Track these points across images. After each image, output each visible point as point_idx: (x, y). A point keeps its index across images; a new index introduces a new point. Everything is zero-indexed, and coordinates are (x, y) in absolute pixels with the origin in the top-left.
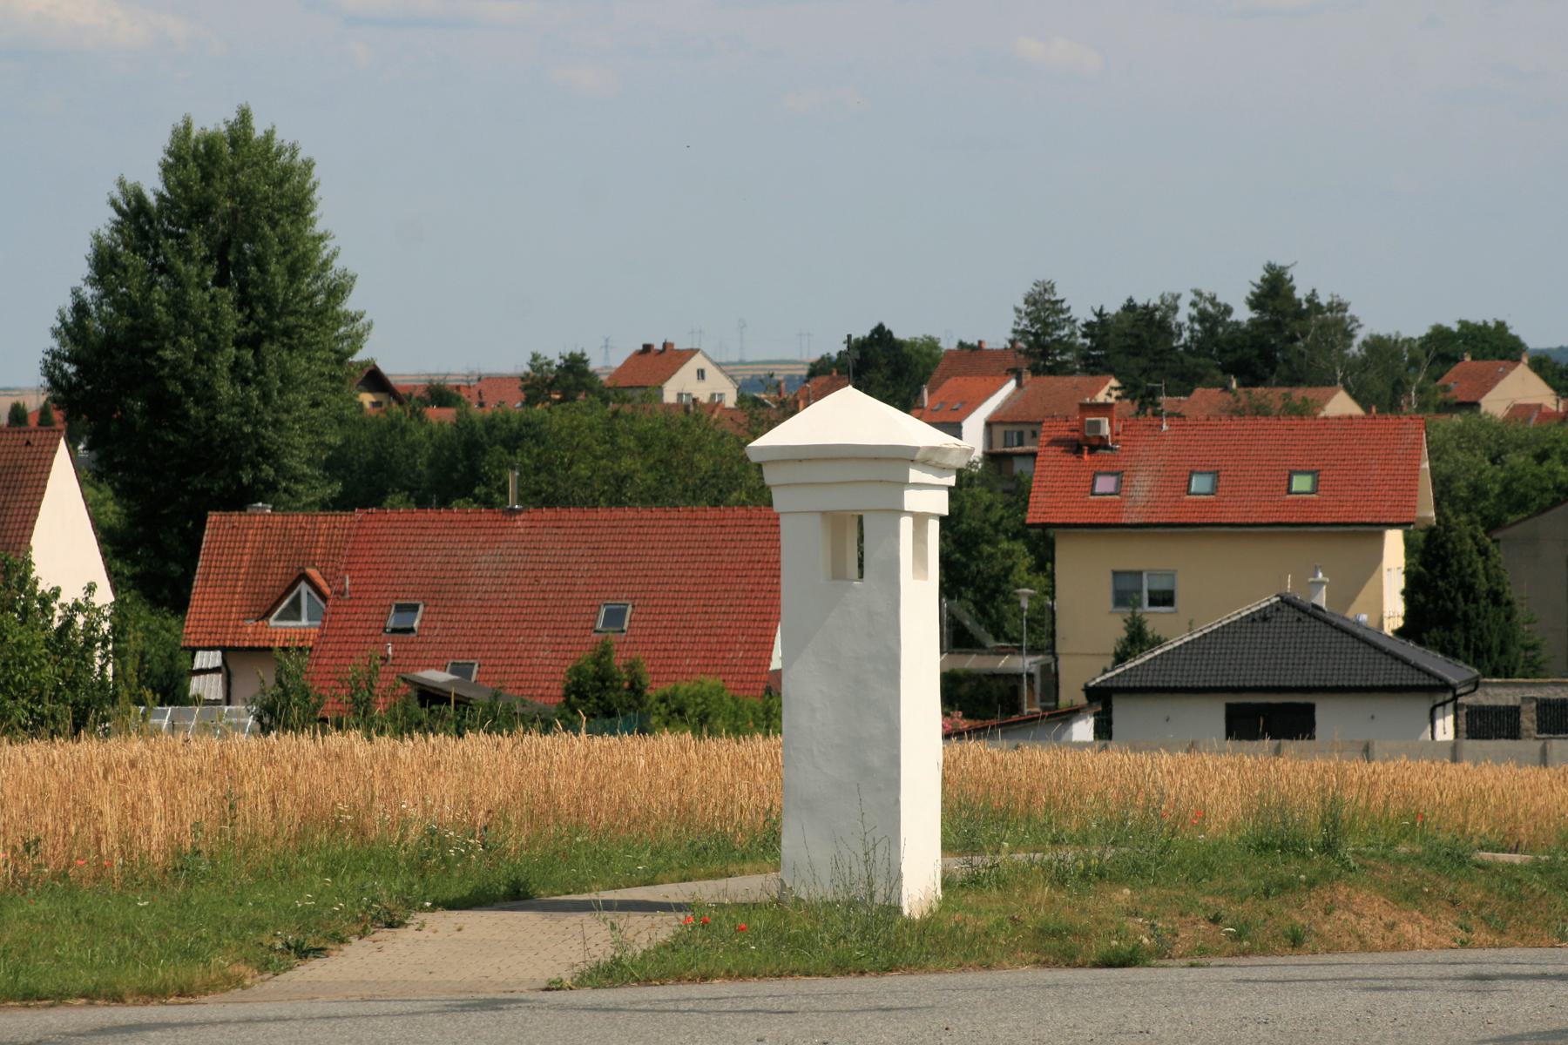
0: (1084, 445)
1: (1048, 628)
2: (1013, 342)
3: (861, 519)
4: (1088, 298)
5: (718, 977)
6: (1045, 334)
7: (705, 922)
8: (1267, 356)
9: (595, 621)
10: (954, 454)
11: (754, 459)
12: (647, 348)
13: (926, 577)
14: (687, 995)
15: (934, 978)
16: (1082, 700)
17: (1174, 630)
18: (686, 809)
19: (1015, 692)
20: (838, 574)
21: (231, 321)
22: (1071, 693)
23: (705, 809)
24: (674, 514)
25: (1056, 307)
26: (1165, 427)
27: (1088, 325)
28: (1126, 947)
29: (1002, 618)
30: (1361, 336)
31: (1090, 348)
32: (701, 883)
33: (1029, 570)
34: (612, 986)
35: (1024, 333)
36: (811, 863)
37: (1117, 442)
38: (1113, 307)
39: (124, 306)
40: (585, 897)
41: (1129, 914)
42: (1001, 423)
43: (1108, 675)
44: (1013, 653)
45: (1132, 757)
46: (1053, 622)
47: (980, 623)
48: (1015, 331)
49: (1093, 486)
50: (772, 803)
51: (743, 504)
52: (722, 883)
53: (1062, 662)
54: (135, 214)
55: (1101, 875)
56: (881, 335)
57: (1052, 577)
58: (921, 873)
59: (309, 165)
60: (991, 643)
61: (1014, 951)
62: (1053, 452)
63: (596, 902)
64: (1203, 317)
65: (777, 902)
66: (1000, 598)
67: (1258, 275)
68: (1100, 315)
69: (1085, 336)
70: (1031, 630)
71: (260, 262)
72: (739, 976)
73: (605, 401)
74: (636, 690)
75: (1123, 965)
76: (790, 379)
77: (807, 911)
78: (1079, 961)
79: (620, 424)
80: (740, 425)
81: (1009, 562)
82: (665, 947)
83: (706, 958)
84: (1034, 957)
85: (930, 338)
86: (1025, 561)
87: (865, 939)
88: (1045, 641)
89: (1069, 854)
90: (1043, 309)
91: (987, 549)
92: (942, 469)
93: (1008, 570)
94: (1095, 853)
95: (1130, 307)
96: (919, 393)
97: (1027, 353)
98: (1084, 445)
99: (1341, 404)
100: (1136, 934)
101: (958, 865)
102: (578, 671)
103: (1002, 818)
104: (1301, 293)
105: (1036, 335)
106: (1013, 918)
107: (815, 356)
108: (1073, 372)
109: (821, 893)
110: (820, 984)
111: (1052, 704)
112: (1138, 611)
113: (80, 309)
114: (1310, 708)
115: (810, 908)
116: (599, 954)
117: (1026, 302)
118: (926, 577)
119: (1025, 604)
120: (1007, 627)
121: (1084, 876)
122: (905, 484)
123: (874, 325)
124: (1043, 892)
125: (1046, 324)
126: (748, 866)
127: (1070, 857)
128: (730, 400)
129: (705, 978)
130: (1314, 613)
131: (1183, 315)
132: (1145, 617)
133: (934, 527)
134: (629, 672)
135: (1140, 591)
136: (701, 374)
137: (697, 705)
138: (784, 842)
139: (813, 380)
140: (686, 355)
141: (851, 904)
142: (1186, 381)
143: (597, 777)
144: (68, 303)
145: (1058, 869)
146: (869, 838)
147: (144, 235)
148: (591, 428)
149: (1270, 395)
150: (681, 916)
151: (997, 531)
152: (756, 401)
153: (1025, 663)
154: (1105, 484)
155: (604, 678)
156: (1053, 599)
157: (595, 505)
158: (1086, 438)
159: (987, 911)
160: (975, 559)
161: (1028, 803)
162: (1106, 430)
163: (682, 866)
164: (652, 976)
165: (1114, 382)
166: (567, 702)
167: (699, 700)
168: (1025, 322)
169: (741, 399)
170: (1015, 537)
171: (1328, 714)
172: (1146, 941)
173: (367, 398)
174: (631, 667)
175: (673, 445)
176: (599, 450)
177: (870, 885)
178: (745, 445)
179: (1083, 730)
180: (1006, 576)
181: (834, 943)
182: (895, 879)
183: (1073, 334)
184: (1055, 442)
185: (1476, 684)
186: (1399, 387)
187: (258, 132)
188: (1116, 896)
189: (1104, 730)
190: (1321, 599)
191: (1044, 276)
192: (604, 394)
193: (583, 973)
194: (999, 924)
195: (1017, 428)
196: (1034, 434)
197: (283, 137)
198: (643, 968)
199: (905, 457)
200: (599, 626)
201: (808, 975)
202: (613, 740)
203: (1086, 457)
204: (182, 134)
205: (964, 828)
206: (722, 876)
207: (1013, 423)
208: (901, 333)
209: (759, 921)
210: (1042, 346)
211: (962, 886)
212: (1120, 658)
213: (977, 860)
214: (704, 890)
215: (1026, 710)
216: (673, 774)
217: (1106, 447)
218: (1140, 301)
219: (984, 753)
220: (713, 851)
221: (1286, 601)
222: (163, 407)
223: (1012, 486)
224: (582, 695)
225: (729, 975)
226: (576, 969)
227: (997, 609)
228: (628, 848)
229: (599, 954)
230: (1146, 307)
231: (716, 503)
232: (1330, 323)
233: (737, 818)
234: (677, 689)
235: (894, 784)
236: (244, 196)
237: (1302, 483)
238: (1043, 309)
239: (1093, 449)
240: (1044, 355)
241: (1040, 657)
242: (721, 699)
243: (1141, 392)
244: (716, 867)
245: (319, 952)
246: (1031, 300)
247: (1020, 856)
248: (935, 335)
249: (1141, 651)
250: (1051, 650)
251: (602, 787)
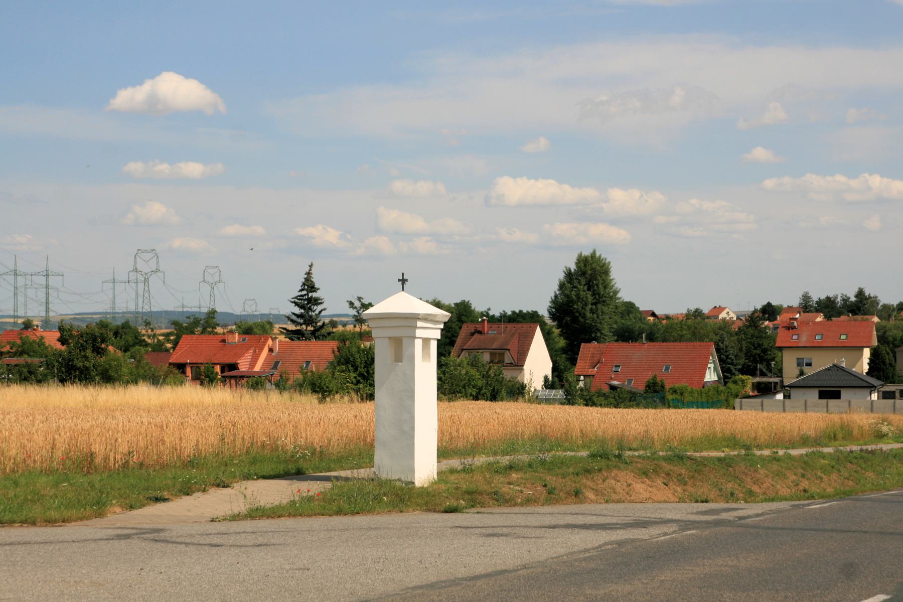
4: (817, 295)
8: (859, 309)
17: (809, 371)
21: (590, 299)
25: (809, 298)
30: (881, 304)
38: (823, 297)
39: (567, 296)
54: (569, 275)
56: (769, 304)
58: (425, 468)
59: (609, 263)
64: (844, 300)
67: (857, 290)
71: (597, 285)
74: (663, 386)
75: (451, 512)
87: (402, 496)
90: (806, 298)
99: (876, 319)
102: (648, 382)
104: (867, 294)
113: (556, 296)
114: (839, 392)
122: (416, 327)
128: (735, 319)
130: (842, 369)
131: (839, 299)
140: (724, 309)
142: (839, 314)
144: (553, 295)
147: (571, 279)
149: (859, 317)
153: (777, 380)
154: (795, 337)
162: (796, 324)
171: (844, 394)
173: (652, 318)
174: (661, 381)
175: (696, 328)
179: (780, 396)
185: (883, 385)
186: (890, 316)
187: (598, 255)
190: (844, 365)
197: (603, 256)
204: (580, 255)
208: (773, 304)
221: (835, 365)
222: (575, 320)
232: (874, 301)
236: (594, 270)
237: (843, 337)
238: (806, 298)
245: (165, 500)
250: (782, 376)
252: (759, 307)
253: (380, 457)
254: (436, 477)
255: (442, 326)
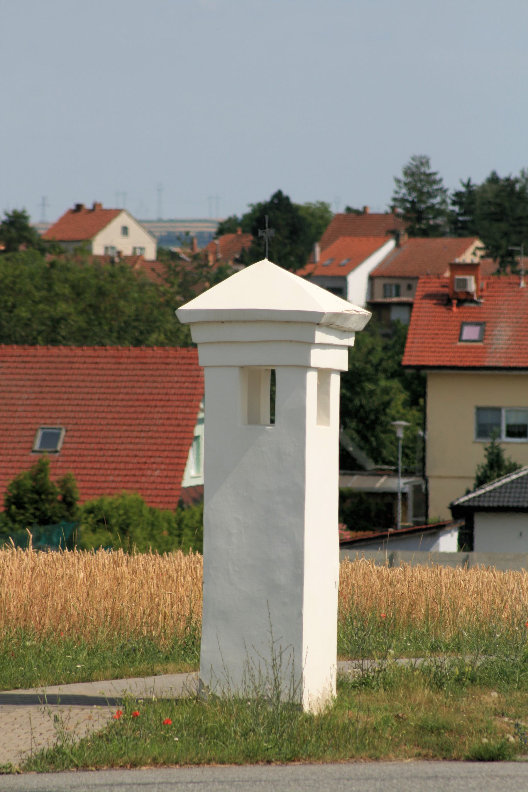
0: (453, 298)
1: (419, 455)
2: (393, 208)
3: (273, 373)
4: (457, 172)
5: (145, 764)
6: (420, 201)
7: (136, 715)
9: (32, 442)
10: (353, 319)
11: (183, 319)
12: (79, 207)
13: (328, 424)
14: (120, 780)
15: (331, 768)
16: (448, 516)
18: (117, 617)
19: (390, 508)
20: (253, 419)
22: (438, 511)
23: (134, 616)
24: (102, 353)
25: (430, 179)
26: (523, 284)
27: (458, 194)
28: (494, 744)
29: (381, 444)
31: (459, 214)
32: (131, 681)
33: (405, 404)
34: (54, 771)
35: (403, 200)
36: (225, 666)
37: (481, 297)
38: (479, 179)
40: (30, 692)
41: (496, 714)
42: (382, 277)
43: (471, 496)
44: (389, 475)
45: (497, 574)
46: (424, 449)
47: (361, 448)
48: (395, 199)
49: (461, 334)
50: (192, 612)
51: (161, 345)
52: (150, 681)
53: (432, 484)
55: (473, 680)
56: (280, 201)
57: (423, 410)
58: (319, 675)
60: (371, 465)
61: (398, 745)
62: (428, 304)
63: (42, 697)
65: (196, 698)
66: (379, 428)
68: (468, 185)
69: (454, 203)
70: (405, 455)
72: (164, 763)
73: (43, 251)
74: (68, 502)
75: (492, 759)
76: (200, 235)
77: (222, 706)
78: (454, 754)
79: (55, 273)
80: (159, 275)
81: (386, 398)
82: (100, 737)
83: (135, 748)
84: (416, 751)
85: (323, 204)
86: (403, 396)
87: (278, 731)
88: (417, 465)
89: (445, 660)
90: (419, 180)
91: (369, 386)
92: (343, 332)
93: (387, 404)
94: (467, 661)
95: (494, 179)
96: (311, 250)
97: (405, 217)
98: (453, 298)
100: (503, 732)
101: (351, 669)
102: (18, 485)
103: (388, 627)
105: (413, 203)
106: (397, 716)
107: (223, 216)
108: (443, 235)
109: (233, 690)
110: (233, 772)
111: (422, 519)
112: (497, 441)
115: (223, 704)
116: (43, 742)
117: (406, 174)
118: (328, 424)
119: (400, 434)
120: (385, 453)
121: (458, 680)
122: (311, 344)
123: (273, 191)
124: (423, 693)
125: (421, 193)
126: (171, 666)
127: (447, 664)
128: (150, 254)
129: (134, 765)
132: (503, 447)
133: (335, 381)
134: (62, 487)
135: (499, 425)
136: (125, 230)
137: (120, 515)
138: (203, 647)
139: (222, 238)
140: (115, 213)
141: (261, 702)
143: (43, 587)
145: (436, 674)
146: (277, 647)
148: (32, 277)
150: (114, 709)
151: (377, 370)
152: (174, 256)
153: (400, 484)
154: (471, 333)
155: (40, 491)
156: (424, 429)
157: (33, 344)
158: (455, 293)
159: (376, 709)
160: (358, 394)
161: (409, 614)
162: (472, 287)
163: (114, 666)
164: (89, 762)
165: (478, 243)
166: (8, 512)
167: (121, 512)
168: (404, 191)
169: (160, 252)
170: (393, 375)
172: (512, 739)
174: (64, 483)
175: (101, 293)
176: (37, 295)
177: (277, 687)
178: (175, 309)
179: (449, 542)
180: (384, 410)
181: (245, 735)
182: (297, 680)
183: (444, 202)
184: (429, 296)
188: (486, 698)
189: (466, 542)
191: (420, 152)
192: (43, 246)
193: (29, 759)
194: (386, 722)
195: (394, 282)
196: (409, 287)
198: (80, 756)
199: (312, 321)
200: (37, 447)
201: (222, 763)
202: (56, 555)
203: (455, 309)
205: (357, 635)
206: (148, 675)
207: (390, 277)
209: (182, 715)
210: (418, 213)
211: (354, 687)
212: (481, 481)
213: (367, 664)
214: (134, 686)
215: (400, 524)
216: (107, 585)
217: (472, 301)
218: (502, 175)
219: (371, 564)
220: (140, 653)
223: (389, 331)
224: (20, 505)
225: (155, 762)
226: (23, 756)
227: (377, 438)
228: (68, 648)
229: (43, 742)
230: (508, 180)
231: (138, 343)
233: (161, 624)
234: (102, 501)
235: (298, 599)
238: (419, 180)
239: (461, 302)
240: (419, 219)
241: (412, 479)
242: (141, 511)
243: (502, 252)
244: (144, 666)
246: (408, 172)
247: (404, 662)
248: (326, 199)
249: (499, 476)
251: (47, 596)
252: (241, 209)
253: (211, 647)
254: (335, 692)
255: (351, 341)
